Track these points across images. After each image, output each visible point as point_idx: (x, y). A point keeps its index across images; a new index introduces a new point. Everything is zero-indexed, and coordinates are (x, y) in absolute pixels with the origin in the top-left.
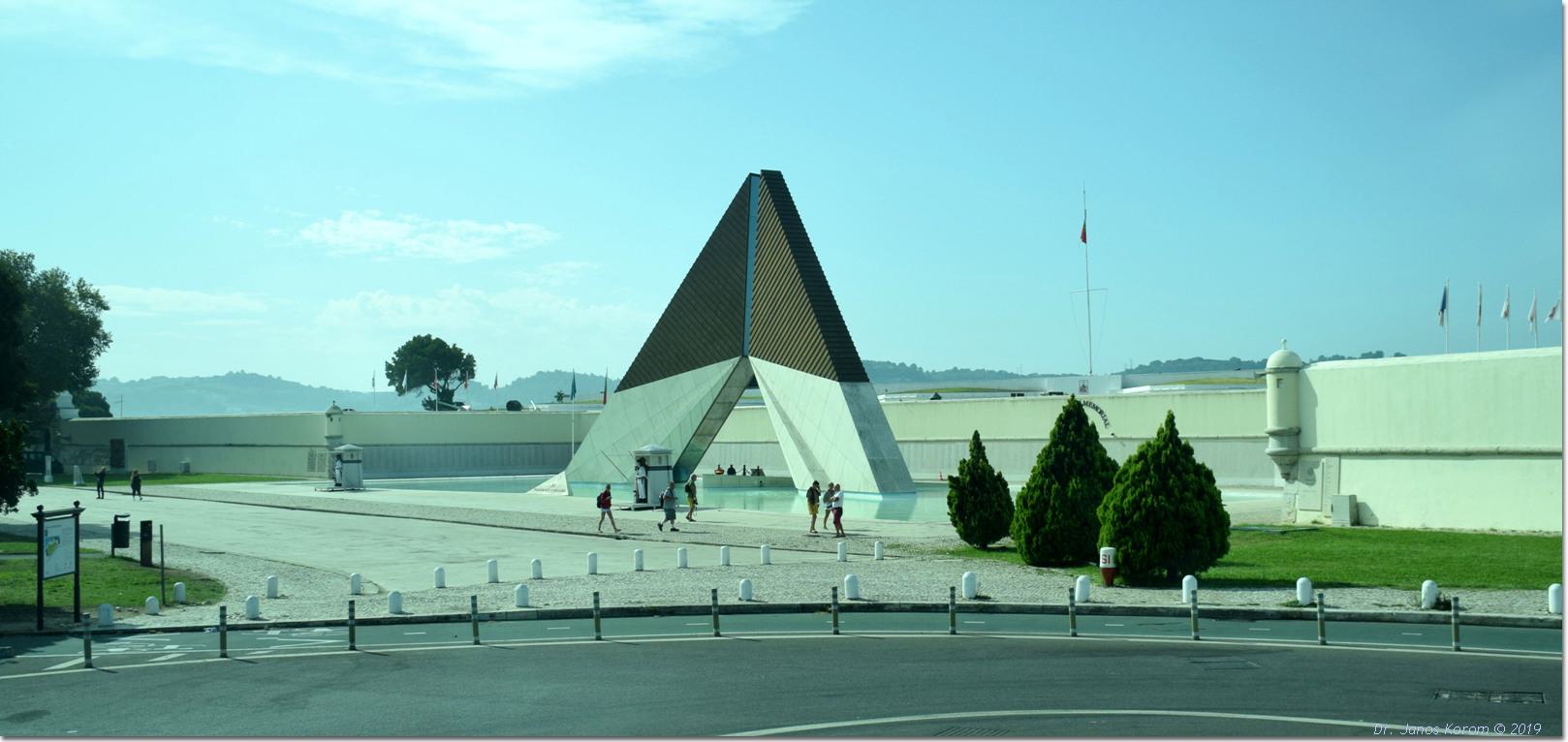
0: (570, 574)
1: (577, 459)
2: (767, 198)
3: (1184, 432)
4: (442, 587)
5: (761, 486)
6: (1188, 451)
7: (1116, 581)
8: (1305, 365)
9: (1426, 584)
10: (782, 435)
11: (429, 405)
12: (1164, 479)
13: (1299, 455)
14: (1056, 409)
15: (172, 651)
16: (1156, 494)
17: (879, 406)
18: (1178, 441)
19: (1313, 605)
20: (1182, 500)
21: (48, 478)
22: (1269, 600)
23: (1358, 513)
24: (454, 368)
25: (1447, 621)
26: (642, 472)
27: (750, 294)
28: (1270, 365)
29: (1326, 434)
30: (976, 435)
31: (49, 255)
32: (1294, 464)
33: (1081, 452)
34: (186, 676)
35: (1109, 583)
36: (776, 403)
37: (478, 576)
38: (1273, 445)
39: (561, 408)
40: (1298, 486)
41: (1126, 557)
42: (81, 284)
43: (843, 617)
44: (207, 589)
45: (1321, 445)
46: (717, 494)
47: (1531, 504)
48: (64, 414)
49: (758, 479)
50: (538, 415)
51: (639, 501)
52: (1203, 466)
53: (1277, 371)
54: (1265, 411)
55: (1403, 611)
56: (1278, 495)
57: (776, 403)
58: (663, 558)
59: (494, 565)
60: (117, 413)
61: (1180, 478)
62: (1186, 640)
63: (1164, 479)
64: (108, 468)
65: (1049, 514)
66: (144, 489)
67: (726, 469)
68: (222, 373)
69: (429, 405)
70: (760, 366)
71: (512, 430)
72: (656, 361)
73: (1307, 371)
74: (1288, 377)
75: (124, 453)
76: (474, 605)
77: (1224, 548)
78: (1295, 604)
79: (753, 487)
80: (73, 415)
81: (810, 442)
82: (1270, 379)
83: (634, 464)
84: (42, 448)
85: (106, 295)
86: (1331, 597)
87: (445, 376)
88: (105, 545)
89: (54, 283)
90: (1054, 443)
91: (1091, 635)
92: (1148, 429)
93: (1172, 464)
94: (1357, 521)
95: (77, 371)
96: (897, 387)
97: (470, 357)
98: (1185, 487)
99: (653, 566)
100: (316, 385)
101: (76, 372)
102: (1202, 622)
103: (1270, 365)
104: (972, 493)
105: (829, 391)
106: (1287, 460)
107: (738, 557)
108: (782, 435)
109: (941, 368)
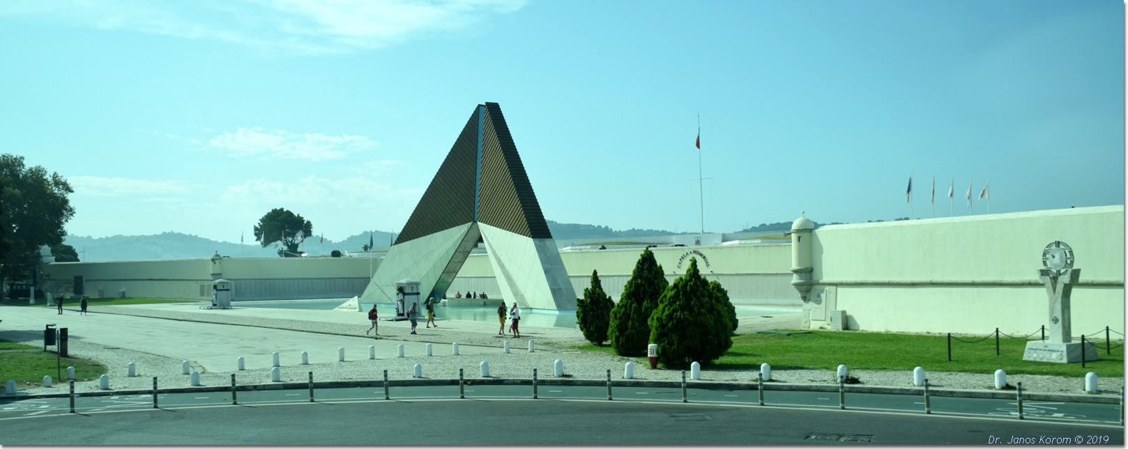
0: (362, 360)
1: (370, 288)
2: (490, 119)
4: (242, 369)
5: (485, 305)
7: (659, 365)
8: (817, 226)
9: (840, 367)
11: (281, 253)
12: (688, 301)
14: (635, 256)
15: (45, 407)
16: (683, 311)
17: (558, 255)
18: (699, 277)
20: (699, 314)
21: (32, 301)
22: (744, 377)
23: (847, 322)
24: (298, 230)
25: (1013, 397)
26: (401, 296)
28: (794, 227)
29: (829, 272)
30: (595, 273)
31: (36, 157)
32: (808, 291)
33: (651, 283)
34: (43, 424)
35: (654, 367)
36: (494, 252)
37: (268, 363)
38: (795, 279)
39: (366, 255)
40: (811, 305)
41: (664, 350)
42: (55, 176)
43: (467, 389)
44: (94, 369)
45: (825, 279)
46: (458, 310)
48: (45, 260)
49: (484, 301)
50: (350, 259)
53: (798, 231)
54: (790, 257)
55: (825, 384)
56: (799, 310)
57: (494, 252)
58: (416, 350)
59: (276, 356)
60: (83, 258)
61: (698, 298)
62: (679, 402)
63: (688, 301)
64: (73, 295)
65: (630, 323)
66: (89, 308)
67: (464, 296)
68: (159, 232)
70: (485, 229)
71: (336, 270)
72: (423, 222)
73: (818, 231)
74: (805, 236)
75: (83, 285)
76: (233, 380)
77: (728, 344)
79: (480, 306)
80: (52, 260)
81: (514, 277)
82: (794, 237)
83: (395, 291)
84: (31, 282)
85: (71, 182)
86: (776, 375)
87: (293, 235)
88: (40, 343)
89: (37, 177)
90: (635, 278)
91: (622, 399)
92: (683, 272)
93: (693, 291)
94: (846, 327)
95: (53, 232)
96: (580, 241)
97: (309, 223)
99: (402, 354)
100: (220, 241)
101: (54, 235)
102: (688, 390)
103: (794, 227)
104: (592, 309)
106: (804, 288)
107: (438, 350)
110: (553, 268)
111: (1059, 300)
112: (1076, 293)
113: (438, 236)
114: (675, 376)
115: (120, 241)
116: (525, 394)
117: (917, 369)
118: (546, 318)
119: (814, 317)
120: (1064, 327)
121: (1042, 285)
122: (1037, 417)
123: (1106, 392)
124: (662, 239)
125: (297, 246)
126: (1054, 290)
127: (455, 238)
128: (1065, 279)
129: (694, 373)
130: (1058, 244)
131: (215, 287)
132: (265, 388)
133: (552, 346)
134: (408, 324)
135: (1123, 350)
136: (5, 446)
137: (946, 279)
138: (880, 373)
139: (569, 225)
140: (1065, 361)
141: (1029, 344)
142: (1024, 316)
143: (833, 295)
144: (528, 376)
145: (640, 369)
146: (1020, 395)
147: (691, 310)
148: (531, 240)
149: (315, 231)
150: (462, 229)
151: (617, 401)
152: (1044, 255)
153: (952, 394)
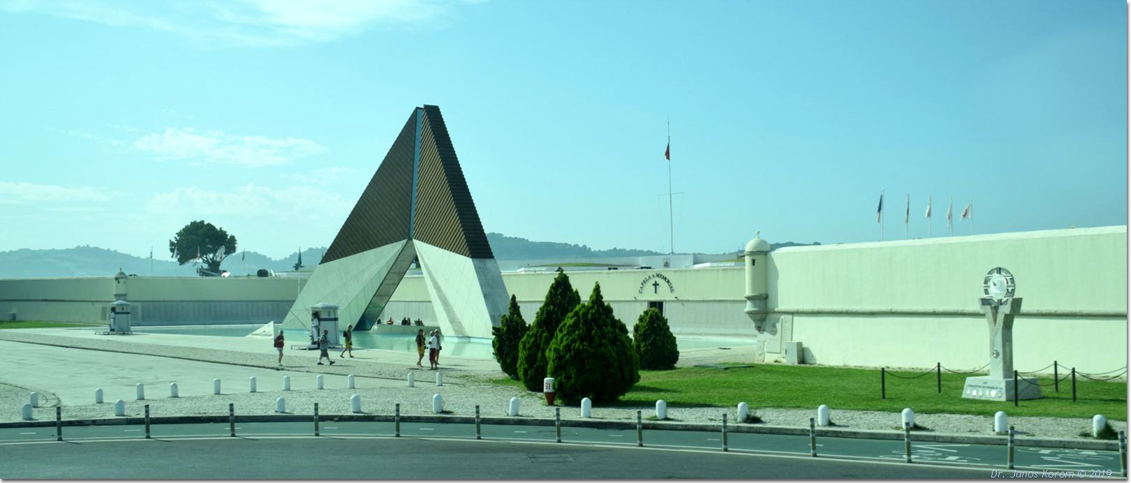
3: (607, 297)
6: (609, 310)
10: (434, 296)
11: (203, 272)
12: (589, 331)
13: (767, 313)
16: (582, 342)
18: (602, 303)
19: (1006, 433)
20: (600, 345)
23: (803, 355)
24: (220, 245)
26: (316, 321)
27: (415, 194)
28: (748, 248)
29: (784, 301)
32: (763, 320)
35: (551, 403)
37: (130, 395)
38: (749, 307)
41: (561, 384)
43: (238, 426)
47: (1101, 354)
50: (279, 281)
51: (314, 343)
52: (619, 321)
53: (752, 253)
55: (713, 423)
61: (599, 327)
63: (589, 331)
67: (398, 322)
68: (72, 246)
69: (203, 272)
70: (421, 247)
71: (260, 291)
72: (355, 236)
73: (773, 254)
74: (759, 259)
78: (655, 418)
81: (451, 301)
86: (674, 413)
87: (215, 252)
90: (547, 304)
93: (595, 320)
94: (802, 360)
97: (233, 237)
98: (604, 336)
105: (464, 265)
106: (759, 317)
108: (434, 296)
109: (605, 247)
110: (491, 287)
111: (1000, 333)
112: (1017, 322)
113: (370, 254)
114: (568, 414)
115: (26, 255)
116: (136, 434)
117: (821, 407)
118: (471, 342)
119: (769, 350)
120: (1005, 362)
121: (983, 315)
122: (929, 460)
123: (1022, 433)
124: (625, 260)
125: (218, 264)
126: (995, 320)
127: (392, 254)
128: (1006, 309)
129: (584, 410)
130: (999, 270)
131: (113, 309)
132: (342, 419)
133: (467, 378)
134: (319, 352)
135: (1126, 390)
136: (5, 480)
137: (906, 308)
138: (791, 412)
139: (542, 243)
140: (1003, 399)
141: (969, 380)
142: (965, 349)
143: (789, 325)
144: (226, 412)
145: (536, 407)
146: (908, 436)
147: (591, 341)
148: (469, 260)
149: (240, 248)
150: (396, 247)
151: (486, 440)
152: (986, 282)
153: (855, 435)
